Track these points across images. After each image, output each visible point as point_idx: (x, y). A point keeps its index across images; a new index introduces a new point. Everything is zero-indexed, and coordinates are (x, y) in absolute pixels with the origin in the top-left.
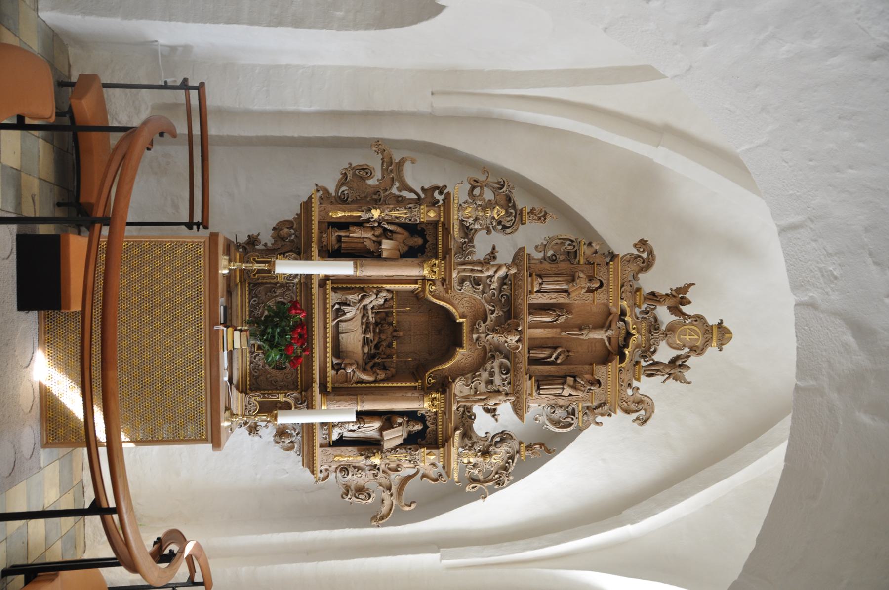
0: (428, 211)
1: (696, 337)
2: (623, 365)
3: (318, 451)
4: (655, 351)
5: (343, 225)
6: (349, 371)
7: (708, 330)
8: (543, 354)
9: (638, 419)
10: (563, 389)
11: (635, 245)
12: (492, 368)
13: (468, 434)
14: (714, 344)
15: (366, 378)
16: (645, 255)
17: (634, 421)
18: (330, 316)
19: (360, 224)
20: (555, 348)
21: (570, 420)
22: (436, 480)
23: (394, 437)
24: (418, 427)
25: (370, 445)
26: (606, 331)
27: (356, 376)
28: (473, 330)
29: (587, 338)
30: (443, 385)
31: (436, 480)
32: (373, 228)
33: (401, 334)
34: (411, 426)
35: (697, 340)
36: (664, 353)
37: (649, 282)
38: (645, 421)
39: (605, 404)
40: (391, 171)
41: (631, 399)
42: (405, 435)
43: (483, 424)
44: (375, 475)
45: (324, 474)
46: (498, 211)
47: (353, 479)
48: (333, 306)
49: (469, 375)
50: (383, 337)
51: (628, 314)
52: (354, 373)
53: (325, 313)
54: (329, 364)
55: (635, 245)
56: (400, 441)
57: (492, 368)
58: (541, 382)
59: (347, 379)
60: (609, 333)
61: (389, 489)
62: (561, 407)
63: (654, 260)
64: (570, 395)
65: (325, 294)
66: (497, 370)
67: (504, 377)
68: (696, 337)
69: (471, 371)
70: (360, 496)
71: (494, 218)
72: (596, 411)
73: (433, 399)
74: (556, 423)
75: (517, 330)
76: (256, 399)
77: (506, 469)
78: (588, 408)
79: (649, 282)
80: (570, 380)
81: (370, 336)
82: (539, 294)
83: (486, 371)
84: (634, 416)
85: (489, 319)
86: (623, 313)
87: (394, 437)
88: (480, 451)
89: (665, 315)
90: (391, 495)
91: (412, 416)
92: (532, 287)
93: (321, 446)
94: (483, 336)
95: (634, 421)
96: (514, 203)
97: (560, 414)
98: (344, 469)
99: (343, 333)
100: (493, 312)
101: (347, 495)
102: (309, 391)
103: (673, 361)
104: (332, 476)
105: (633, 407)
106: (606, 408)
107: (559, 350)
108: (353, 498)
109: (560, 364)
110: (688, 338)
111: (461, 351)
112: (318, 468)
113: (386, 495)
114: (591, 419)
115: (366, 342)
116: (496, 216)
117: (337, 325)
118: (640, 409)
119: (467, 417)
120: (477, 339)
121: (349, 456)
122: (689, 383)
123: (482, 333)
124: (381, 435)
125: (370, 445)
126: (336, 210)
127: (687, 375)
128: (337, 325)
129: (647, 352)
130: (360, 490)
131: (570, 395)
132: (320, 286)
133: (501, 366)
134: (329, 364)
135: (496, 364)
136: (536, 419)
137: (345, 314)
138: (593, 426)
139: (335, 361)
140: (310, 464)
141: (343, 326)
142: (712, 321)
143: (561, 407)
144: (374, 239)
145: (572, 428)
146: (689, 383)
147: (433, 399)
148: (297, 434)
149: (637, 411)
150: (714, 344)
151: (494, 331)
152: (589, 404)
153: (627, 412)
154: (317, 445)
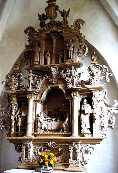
0: (13, 100)
1: (52, 9)
2: (64, 32)
3: (94, 138)
4: (59, 22)
5: (17, 128)
6: (64, 126)
7: (50, 6)
8: (60, 59)
9: (82, 24)
10: (70, 50)
11: (26, 34)
12: (65, 76)
13: (88, 83)
14: (54, 3)
15: (67, 120)
16: (29, 30)
17: (83, 25)
18: (46, 133)
19: (16, 122)
20: (59, 55)
21: (83, 47)
22: (106, 93)
23: (87, 109)
24: (85, 100)
25: (92, 119)
26: (53, 39)
27: (66, 123)
28: (52, 84)
29: (55, 45)
30: (70, 92)
31: (106, 93)
32: (18, 118)
33: (56, 108)
34: (84, 103)
35: (53, 8)
36: (59, 18)
37: (37, 28)
38: (83, 21)
39: (77, 36)
40: (2, 113)
41: (75, 27)
42: (88, 105)
43: (85, 77)
44: (104, 116)
45: (104, 135)
46: (13, 78)
47: (106, 124)
48: (44, 132)
49: (67, 83)
50: (57, 114)
51: (47, 32)
52: (65, 124)
53: (46, 135)
54: (62, 133)
55: (26, 34)
56: (90, 107)
57: (65, 76)
58: (68, 58)
59: (67, 127)
60: (54, 38)
61: (109, 110)
62: (79, 51)
63: (30, 27)
64: (73, 47)
65: (38, 135)
66: (65, 74)
67: (68, 71)
68: (52, 9)
69: (66, 83)
70: (112, 121)
71: (15, 79)
72: (80, 39)
73: (74, 95)
74: (84, 52)
75: (50, 68)
76: (71, 161)
77: (101, 68)
78: (79, 42)
79: (37, 28)
80: (67, 48)
81: (54, 119)
82: (41, 62)
83: (65, 78)
84: (81, 25)
85: (48, 78)
86: (47, 34)
87: (87, 109)
88: (92, 77)
89: (48, 21)
90: (112, 110)
91: (82, 103)
92: (37, 64)
93: (92, 137)
94: (54, 79)
95: (83, 25)
96: (13, 73)
97: (81, 51)
98: (102, 128)
99: (52, 129)
100: (46, 77)
101: (112, 127)
102: (69, 141)
103: (62, 15)
104: (104, 132)
105: (78, 26)
106: (79, 36)
107: (59, 54)
108: (112, 124)
109: (63, 52)
110: (53, 12)
111: (59, 87)
112: (101, 138)
113: (112, 112)
114: (83, 40)
115: (56, 121)
116: (14, 78)
117: (49, 130)
118: (79, 23)
119: (82, 83)
120: (55, 81)
121: (96, 126)
122: (69, 9)
123: (53, 80)
124: (87, 114)
125: (92, 119)
126: (12, 131)
127: (67, 10)
128: (49, 130)
129: (59, 25)
130: (110, 122)
131: (73, 47)
132: (36, 137)
133: (64, 73)
134: (62, 133)
135: (63, 75)
136: (83, 59)
137: (45, 128)
138: (39, 19)
139: (62, 131)
140: (99, 141)
141: (50, 128)
142: (47, 5)
143: (79, 51)
144: (21, 118)
145: (86, 46)
146: (69, 9)
147: (74, 95)
148: (87, 145)
149: (79, 24)
150: (54, 3)
151: (52, 76)
152: (78, 41)
153: (80, 28)
154: (92, 138)
